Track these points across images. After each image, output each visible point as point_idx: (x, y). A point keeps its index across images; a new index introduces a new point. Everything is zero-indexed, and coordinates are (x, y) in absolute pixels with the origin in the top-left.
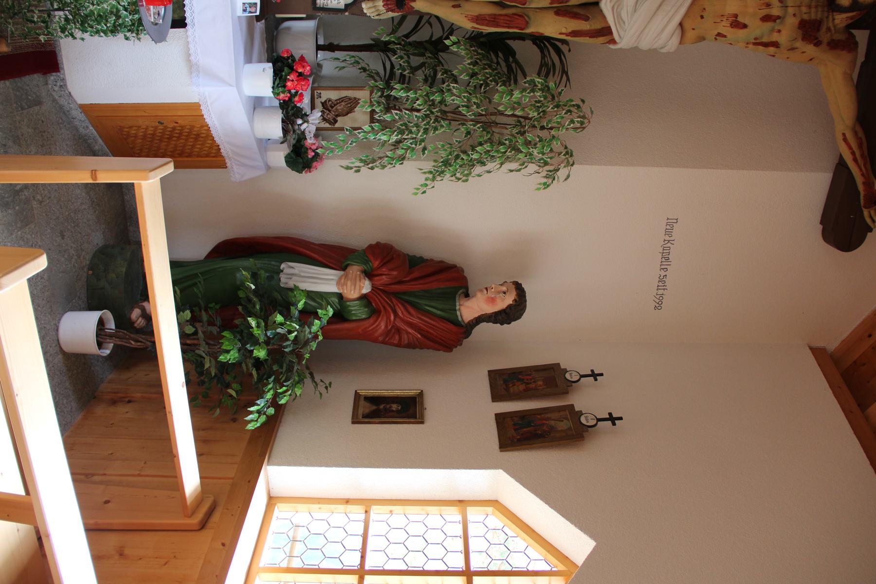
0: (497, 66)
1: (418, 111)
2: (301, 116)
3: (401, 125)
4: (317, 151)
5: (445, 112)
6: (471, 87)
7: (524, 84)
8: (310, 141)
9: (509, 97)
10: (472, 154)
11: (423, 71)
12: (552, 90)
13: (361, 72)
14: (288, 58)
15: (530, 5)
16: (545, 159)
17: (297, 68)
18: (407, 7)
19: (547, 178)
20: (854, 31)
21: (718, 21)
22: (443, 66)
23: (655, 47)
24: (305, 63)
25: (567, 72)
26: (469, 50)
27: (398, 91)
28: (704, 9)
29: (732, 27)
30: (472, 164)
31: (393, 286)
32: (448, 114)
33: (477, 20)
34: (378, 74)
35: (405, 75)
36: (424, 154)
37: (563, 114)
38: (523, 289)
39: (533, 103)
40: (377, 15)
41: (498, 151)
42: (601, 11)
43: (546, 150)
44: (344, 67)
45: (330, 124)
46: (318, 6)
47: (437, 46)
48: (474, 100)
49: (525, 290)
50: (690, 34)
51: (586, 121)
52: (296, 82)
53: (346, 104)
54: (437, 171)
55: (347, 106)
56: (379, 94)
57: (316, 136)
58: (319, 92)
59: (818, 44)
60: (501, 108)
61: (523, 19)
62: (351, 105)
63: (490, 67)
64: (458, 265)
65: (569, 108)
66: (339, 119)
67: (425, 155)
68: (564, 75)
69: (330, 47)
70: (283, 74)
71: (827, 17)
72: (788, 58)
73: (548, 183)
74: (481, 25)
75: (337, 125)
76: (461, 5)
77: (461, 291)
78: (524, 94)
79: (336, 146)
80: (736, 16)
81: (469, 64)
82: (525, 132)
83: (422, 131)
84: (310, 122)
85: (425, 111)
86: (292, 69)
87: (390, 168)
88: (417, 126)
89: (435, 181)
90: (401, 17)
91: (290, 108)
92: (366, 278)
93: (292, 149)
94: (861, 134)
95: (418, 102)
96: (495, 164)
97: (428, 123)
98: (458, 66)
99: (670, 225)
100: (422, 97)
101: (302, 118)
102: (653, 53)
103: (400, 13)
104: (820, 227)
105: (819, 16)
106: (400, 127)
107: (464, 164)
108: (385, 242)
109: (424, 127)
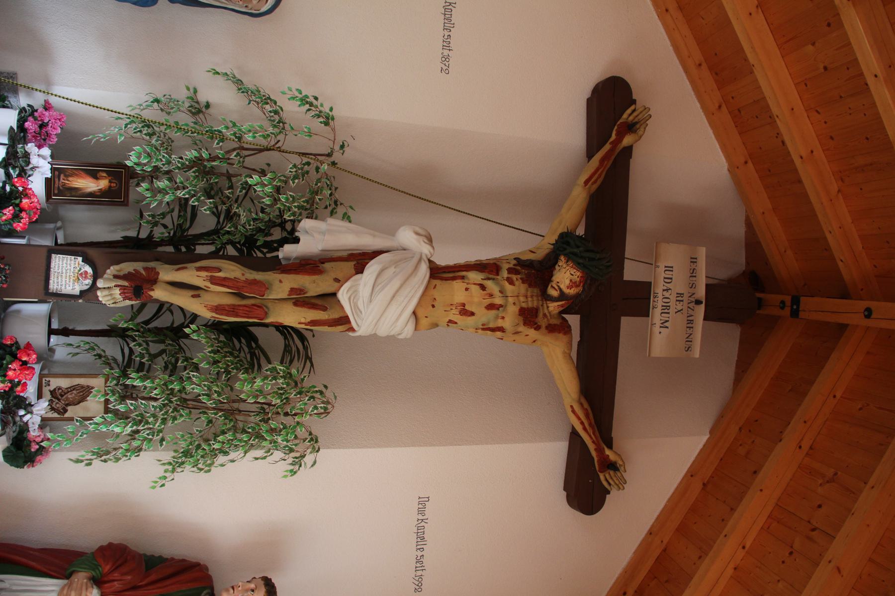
0: (240, 353)
1: (155, 399)
2: (25, 407)
3: (136, 415)
4: (41, 444)
5: (186, 400)
6: (213, 375)
7: (265, 372)
8: (34, 432)
9: (250, 385)
10: (214, 444)
11: (163, 358)
12: (294, 376)
13: (96, 359)
14: (12, 345)
15: (268, 296)
16: (290, 446)
17: (20, 356)
18: (146, 296)
19: (293, 465)
20: (564, 316)
21: (448, 309)
22: (185, 354)
23: (392, 333)
24: (31, 351)
25: (311, 358)
26: (210, 338)
27: (135, 380)
28: (435, 299)
29: (461, 315)
30: (214, 454)
31: (127, 593)
32: (188, 402)
33: (216, 310)
34: (115, 360)
35: (144, 363)
36: (161, 445)
37: (306, 400)
38: (274, 584)
39: (275, 391)
40: (113, 303)
41: (241, 440)
42: (339, 301)
43: (290, 437)
44: (78, 354)
45: (59, 414)
46: (50, 291)
47: (177, 333)
48: (215, 388)
49: (276, 585)
50: (424, 322)
51: (329, 406)
52: (19, 372)
53: (78, 393)
54: (177, 462)
55: (78, 395)
56: (115, 382)
57: (41, 427)
58: (47, 379)
59: (538, 328)
60: (243, 396)
61: (262, 309)
62: (84, 393)
63: (232, 354)
64: (202, 564)
65: (312, 395)
66: (69, 408)
67: (163, 446)
68: (308, 361)
69: (65, 332)
70: (5, 362)
71: (542, 305)
72: (514, 341)
73: (294, 470)
74: (220, 315)
75: (67, 415)
76: (200, 295)
77: (205, 592)
78: (266, 381)
79: (65, 438)
80: (464, 305)
81: (209, 352)
82: (269, 419)
83: (159, 421)
84: (35, 412)
85: (163, 401)
86: (15, 357)
87: (125, 461)
88: (154, 416)
89: (175, 474)
90: (141, 305)
91: (11, 398)
92: (95, 586)
93: (11, 442)
94: (586, 406)
95: (155, 392)
96: (238, 453)
97: (166, 413)
98: (198, 355)
99: (423, 503)
100: (160, 386)
101: (25, 409)
102: (391, 339)
103: (138, 302)
104: (565, 493)
105: (535, 304)
106: (136, 417)
107: (206, 454)
108: (119, 542)
109: (162, 417)
